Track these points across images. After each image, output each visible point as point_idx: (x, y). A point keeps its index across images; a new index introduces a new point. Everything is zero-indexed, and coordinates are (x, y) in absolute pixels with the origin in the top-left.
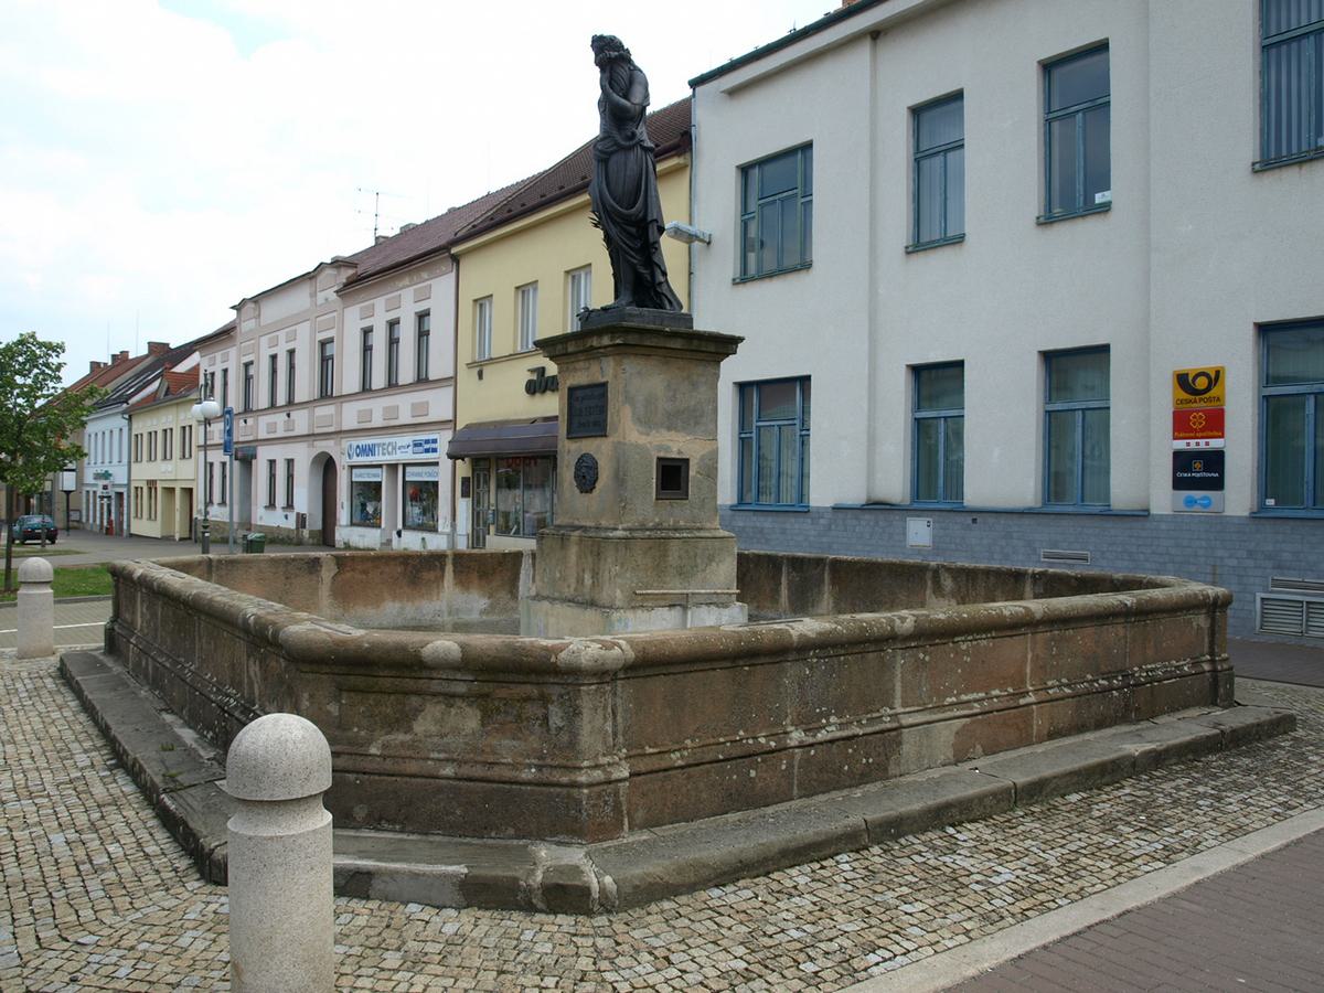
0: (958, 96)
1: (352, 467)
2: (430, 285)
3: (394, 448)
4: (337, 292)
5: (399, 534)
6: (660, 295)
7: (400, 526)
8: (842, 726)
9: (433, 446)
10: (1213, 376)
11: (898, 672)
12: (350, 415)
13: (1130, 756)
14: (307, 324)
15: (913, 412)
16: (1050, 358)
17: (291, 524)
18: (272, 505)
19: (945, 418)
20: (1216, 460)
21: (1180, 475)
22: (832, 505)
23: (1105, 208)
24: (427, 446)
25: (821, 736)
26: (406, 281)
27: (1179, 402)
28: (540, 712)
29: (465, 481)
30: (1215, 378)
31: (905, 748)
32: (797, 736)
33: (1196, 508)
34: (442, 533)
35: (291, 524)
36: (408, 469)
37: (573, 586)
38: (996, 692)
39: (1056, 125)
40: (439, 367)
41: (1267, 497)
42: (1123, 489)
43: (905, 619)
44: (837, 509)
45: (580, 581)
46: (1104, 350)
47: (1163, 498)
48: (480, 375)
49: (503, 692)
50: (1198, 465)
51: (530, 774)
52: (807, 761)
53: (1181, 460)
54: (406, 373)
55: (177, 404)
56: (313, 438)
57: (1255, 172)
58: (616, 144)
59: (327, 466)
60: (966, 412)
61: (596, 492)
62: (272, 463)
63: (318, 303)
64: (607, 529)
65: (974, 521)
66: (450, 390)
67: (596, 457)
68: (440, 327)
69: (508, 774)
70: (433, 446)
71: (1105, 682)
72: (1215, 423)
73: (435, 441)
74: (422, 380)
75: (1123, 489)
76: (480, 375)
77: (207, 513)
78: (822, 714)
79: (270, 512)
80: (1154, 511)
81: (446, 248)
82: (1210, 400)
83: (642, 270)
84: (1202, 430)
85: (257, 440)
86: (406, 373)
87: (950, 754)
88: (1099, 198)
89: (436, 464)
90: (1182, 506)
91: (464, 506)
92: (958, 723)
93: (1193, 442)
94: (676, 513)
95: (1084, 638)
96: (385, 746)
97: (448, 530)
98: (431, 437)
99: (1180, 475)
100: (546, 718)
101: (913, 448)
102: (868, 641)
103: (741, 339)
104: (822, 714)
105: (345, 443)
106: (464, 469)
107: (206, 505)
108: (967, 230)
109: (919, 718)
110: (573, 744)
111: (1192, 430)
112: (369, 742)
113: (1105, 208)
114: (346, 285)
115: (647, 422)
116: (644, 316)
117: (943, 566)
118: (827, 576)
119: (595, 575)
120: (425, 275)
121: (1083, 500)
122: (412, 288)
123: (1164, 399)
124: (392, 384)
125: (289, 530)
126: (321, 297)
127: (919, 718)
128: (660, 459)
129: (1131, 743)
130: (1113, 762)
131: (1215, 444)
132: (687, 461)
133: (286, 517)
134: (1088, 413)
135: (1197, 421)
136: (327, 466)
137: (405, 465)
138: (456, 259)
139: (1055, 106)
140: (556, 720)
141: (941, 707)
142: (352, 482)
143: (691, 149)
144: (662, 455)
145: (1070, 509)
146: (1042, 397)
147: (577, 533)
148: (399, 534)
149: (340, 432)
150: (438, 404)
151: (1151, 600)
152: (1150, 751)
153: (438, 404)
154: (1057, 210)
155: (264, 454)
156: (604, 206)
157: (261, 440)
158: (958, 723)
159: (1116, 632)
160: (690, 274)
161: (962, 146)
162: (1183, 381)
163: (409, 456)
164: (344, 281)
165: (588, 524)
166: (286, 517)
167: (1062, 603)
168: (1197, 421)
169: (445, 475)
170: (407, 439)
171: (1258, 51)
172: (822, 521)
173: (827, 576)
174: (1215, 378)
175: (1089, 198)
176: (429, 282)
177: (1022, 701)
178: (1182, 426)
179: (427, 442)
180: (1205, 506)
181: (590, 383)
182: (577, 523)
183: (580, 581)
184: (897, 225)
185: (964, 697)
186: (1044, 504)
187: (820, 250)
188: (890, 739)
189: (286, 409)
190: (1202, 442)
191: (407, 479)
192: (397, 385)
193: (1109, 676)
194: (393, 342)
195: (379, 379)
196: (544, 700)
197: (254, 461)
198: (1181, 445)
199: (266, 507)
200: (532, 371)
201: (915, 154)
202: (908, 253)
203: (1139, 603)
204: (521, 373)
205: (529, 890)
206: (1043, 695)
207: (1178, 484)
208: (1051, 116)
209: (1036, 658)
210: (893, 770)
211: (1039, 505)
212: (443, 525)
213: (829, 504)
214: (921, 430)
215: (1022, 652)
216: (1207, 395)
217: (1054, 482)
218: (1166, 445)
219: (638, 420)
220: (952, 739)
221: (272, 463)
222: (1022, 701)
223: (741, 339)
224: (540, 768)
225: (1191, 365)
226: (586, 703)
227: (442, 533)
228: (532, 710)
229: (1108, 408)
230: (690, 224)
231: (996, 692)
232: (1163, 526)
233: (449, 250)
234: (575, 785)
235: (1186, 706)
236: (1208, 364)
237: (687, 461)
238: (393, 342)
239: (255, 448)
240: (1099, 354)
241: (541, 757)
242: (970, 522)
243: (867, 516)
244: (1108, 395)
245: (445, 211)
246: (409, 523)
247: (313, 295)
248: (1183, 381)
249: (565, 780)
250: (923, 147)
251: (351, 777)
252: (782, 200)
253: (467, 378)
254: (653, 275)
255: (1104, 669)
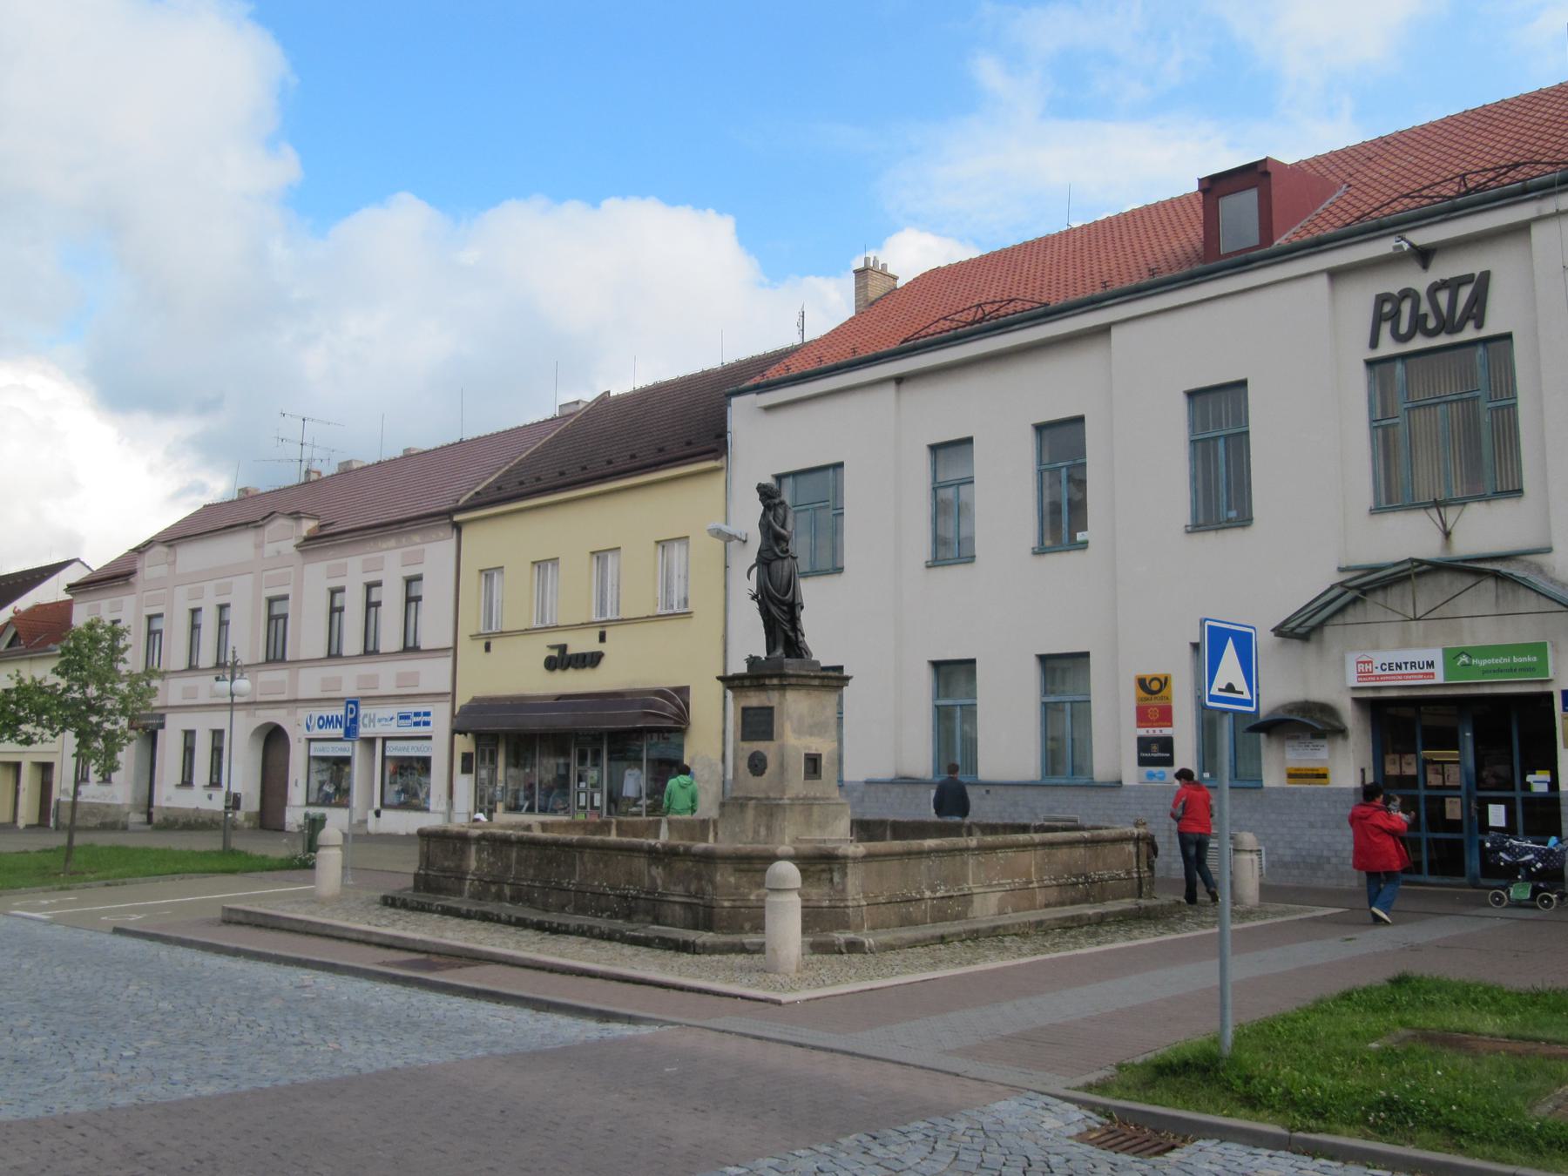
0: (969, 441)
1: (310, 740)
2: (424, 550)
3: (371, 721)
4: (297, 546)
5: (378, 814)
6: (800, 649)
7: (377, 805)
8: (947, 891)
9: (426, 719)
10: (1163, 681)
11: (970, 866)
12: (310, 682)
13: (1087, 915)
14: (249, 578)
15: (933, 700)
16: (1043, 659)
17: (217, 803)
18: (187, 782)
19: (961, 706)
20: (1167, 744)
21: (1143, 755)
22: (865, 779)
23: (1084, 545)
24: (418, 719)
25: (938, 895)
26: (392, 542)
27: (1140, 699)
28: (829, 876)
29: (466, 758)
30: (1164, 682)
31: (975, 904)
32: (928, 894)
33: (1155, 780)
34: (435, 812)
35: (217, 803)
36: (388, 743)
37: (750, 836)
38: (1017, 880)
39: (1046, 475)
40: (434, 631)
41: (1204, 771)
42: (1101, 769)
43: (973, 842)
44: (869, 783)
45: (756, 832)
46: (1086, 655)
47: (1132, 774)
48: (488, 648)
49: (812, 869)
50: (1155, 747)
51: (826, 903)
52: (933, 906)
53: (1144, 744)
54: (390, 638)
55: (31, 659)
56: (254, 707)
57: (1188, 532)
58: (776, 554)
59: (273, 739)
60: (979, 702)
61: (765, 776)
62: (189, 735)
63: (266, 556)
64: (775, 799)
65: (988, 792)
66: (450, 660)
67: (766, 753)
68: (435, 595)
69: (816, 904)
70: (426, 719)
71: (1074, 880)
72: (1166, 716)
73: (427, 714)
74: (410, 648)
75: (1101, 769)
76: (488, 648)
77: (76, 793)
78: (938, 885)
79: (185, 792)
80: (1125, 782)
81: (449, 513)
82: (1162, 698)
83: (791, 634)
84: (1157, 721)
85: (166, 707)
86: (390, 638)
87: (996, 910)
88: (1080, 536)
89: (429, 738)
90: (1144, 778)
91: (465, 784)
92: (999, 894)
93: (1151, 730)
94: (814, 788)
95: (1063, 854)
96: (758, 896)
97: (443, 807)
98: (422, 709)
99: (1143, 755)
100: (831, 880)
101: (934, 730)
102: (956, 850)
103: (851, 677)
104: (938, 885)
105: (303, 714)
106: (464, 744)
107: (77, 784)
108: (977, 553)
109: (981, 890)
110: (844, 890)
111: (1152, 721)
112: (749, 894)
113: (1084, 545)
114: (308, 539)
115: (799, 732)
116: (792, 666)
117: (974, 824)
118: (888, 832)
119: (769, 828)
120: (416, 538)
121: (1073, 774)
122: (400, 551)
123: (1130, 697)
124: (370, 651)
125: (214, 812)
126: (269, 549)
127: (981, 890)
128: (806, 755)
129: (1088, 910)
130: (1078, 916)
131: (1166, 731)
132: (820, 755)
133: (210, 797)
134: (1076, 705)
135: (1154, 714)
136: (273, 739)
137: (385, 739)
138: (458, 527)
139: (1046, 460)
140: (837, 878)
141: (990, 886)
142: (309, 757)
143: (727, 454)
144: (807, 751)
145: (1063, 781)
146: (1039, 693)
147: (753, 802)
148: (378, 814)
149: (295, 701)
150: (432, 674)
151: (1099, 835)
152: (1097, 913)
153: (432, 674)
154: (1048, 543)
155: (173, 730)
156: (767, 592)
157: (172, 707)
158: (999, 894)
159: (1080, 851)
160: (726, 567)
161: (972, 482)
162: (1142, 683)
163: (393, 729)
164: (305, 534)
165: (759, 796)
166: (210, 797)
167: (1049, 836)
168: (1154, 714)
169: (440, 744)
170: (393, 710)
171: (1188, 443)
172: (855, 794)
173: (888, 832)
174: (1164, 682)
175: (1072, 537)
176: (421, 547)
177: (1031, 886)
178: (1143, 717)
179: (417, 714)
180: (1161, 778)
181: (761, 705)
182: (749, 795)
183: (756, 832)
184: (920, 544)
185: (1001, 882)
186: (1043, 777)
187: (851, 555)
188: (967, 898)
189: (213, 672)
190: (1157, 730)
191: (388, 754)
192: (376, 652)
193: (1077, 876)
194: (371, 606)
195: (352, 643)
196: (831, 871)
197: (160, 732)
198: (1143, 732)
199: (177, 786)
200: (552, 647)
201: (933, 484)
202: (928, 567)
203: (1092, 836)
204: (541, 648)
205: (840, 945)
206: (1041, 884)
207: (1142, 762)
208: (1044, 467)
209: (1036, 864)
210: (970, 915)
211: (1039, 778)
212: (437, 800)
213: (861, 778)
214: (943, 716)
215: (1030, 859)
216: (1160, 695)
217: (1053, 757)
218: (1132, 732)
219: (794, 731)
220: (997, 902)
221: (189, 735)
222: (1031, 886)
223: (851, 677)
224: (830, 901)
225: (1148, 671)
226: (849, 871)
227: (435, 812)
228: (825, 876)
229: (1089, 701)
230: (726, 523)
231: (1017, 880)
232: (1133, 794)
233: (451, 517)
234: (847, 907)
235: (1123, 897)
236: (1159, 671)
237: (820, 755)
238: (371, 606)
239: (162, 716)
240: (1081, 658)
241: (830, 896)
242: (984, 792)
243: (897, 790)
244: (1089, 691)
245: (399, 454)
246: (387, 801)
247: (259, 546)
248: (1142, 683)
249: (842, 905)
250: (940, 478)
251: (743, 910)
252: (814, 509)
253: (470, 652)
254: (796, 637)
255: (1074, 872)
